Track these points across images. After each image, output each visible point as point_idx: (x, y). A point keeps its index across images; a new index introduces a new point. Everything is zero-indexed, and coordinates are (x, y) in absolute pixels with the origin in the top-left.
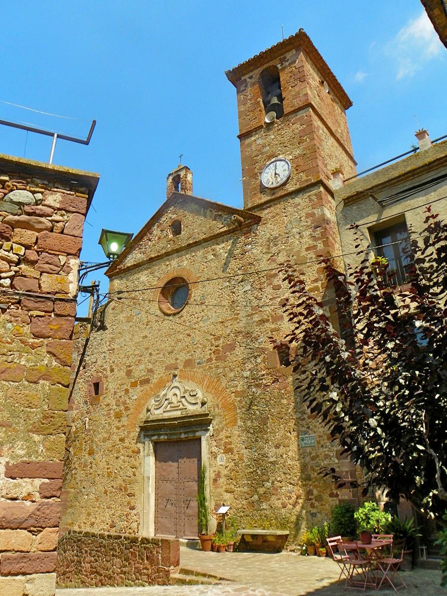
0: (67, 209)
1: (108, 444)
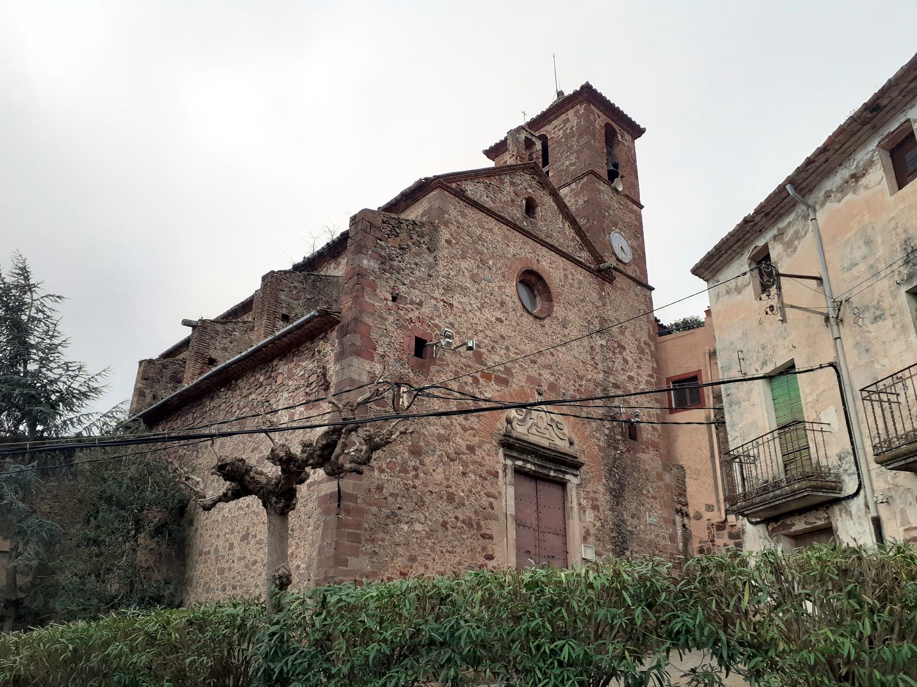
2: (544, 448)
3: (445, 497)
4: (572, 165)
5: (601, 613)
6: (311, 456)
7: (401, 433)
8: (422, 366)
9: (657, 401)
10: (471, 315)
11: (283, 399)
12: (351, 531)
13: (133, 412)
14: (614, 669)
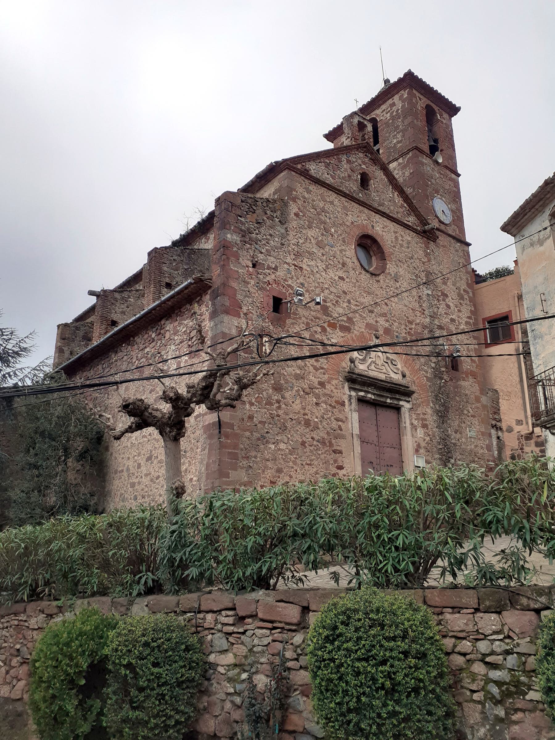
2: (381, 381)
3: (303, 423)
4: (398, 142)
5: (428, 509)
6: (194, 395)
7: (264, 375)
8: (279, 319)
9: (475, 338)
10: (318, 275)
11: (171, 351)
12: (230, 451)
13: (55, 365)
14: (439, 551)
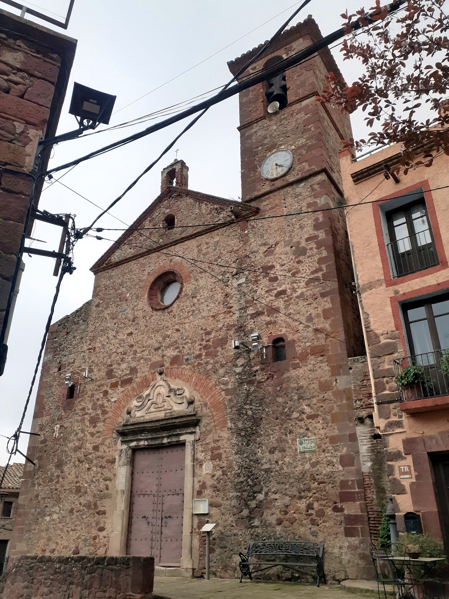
0: (31, 72)
1: (80, 454)
2: (162, 420)
